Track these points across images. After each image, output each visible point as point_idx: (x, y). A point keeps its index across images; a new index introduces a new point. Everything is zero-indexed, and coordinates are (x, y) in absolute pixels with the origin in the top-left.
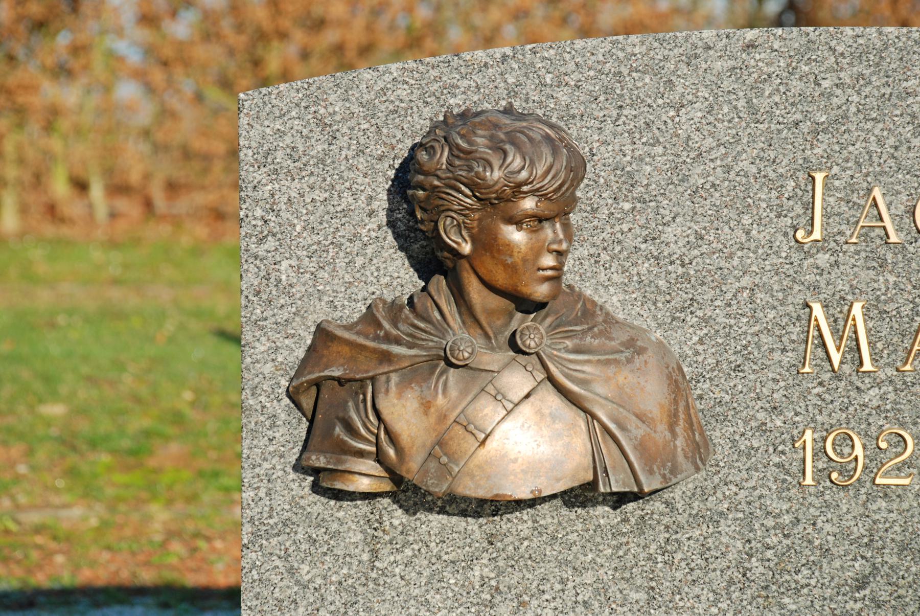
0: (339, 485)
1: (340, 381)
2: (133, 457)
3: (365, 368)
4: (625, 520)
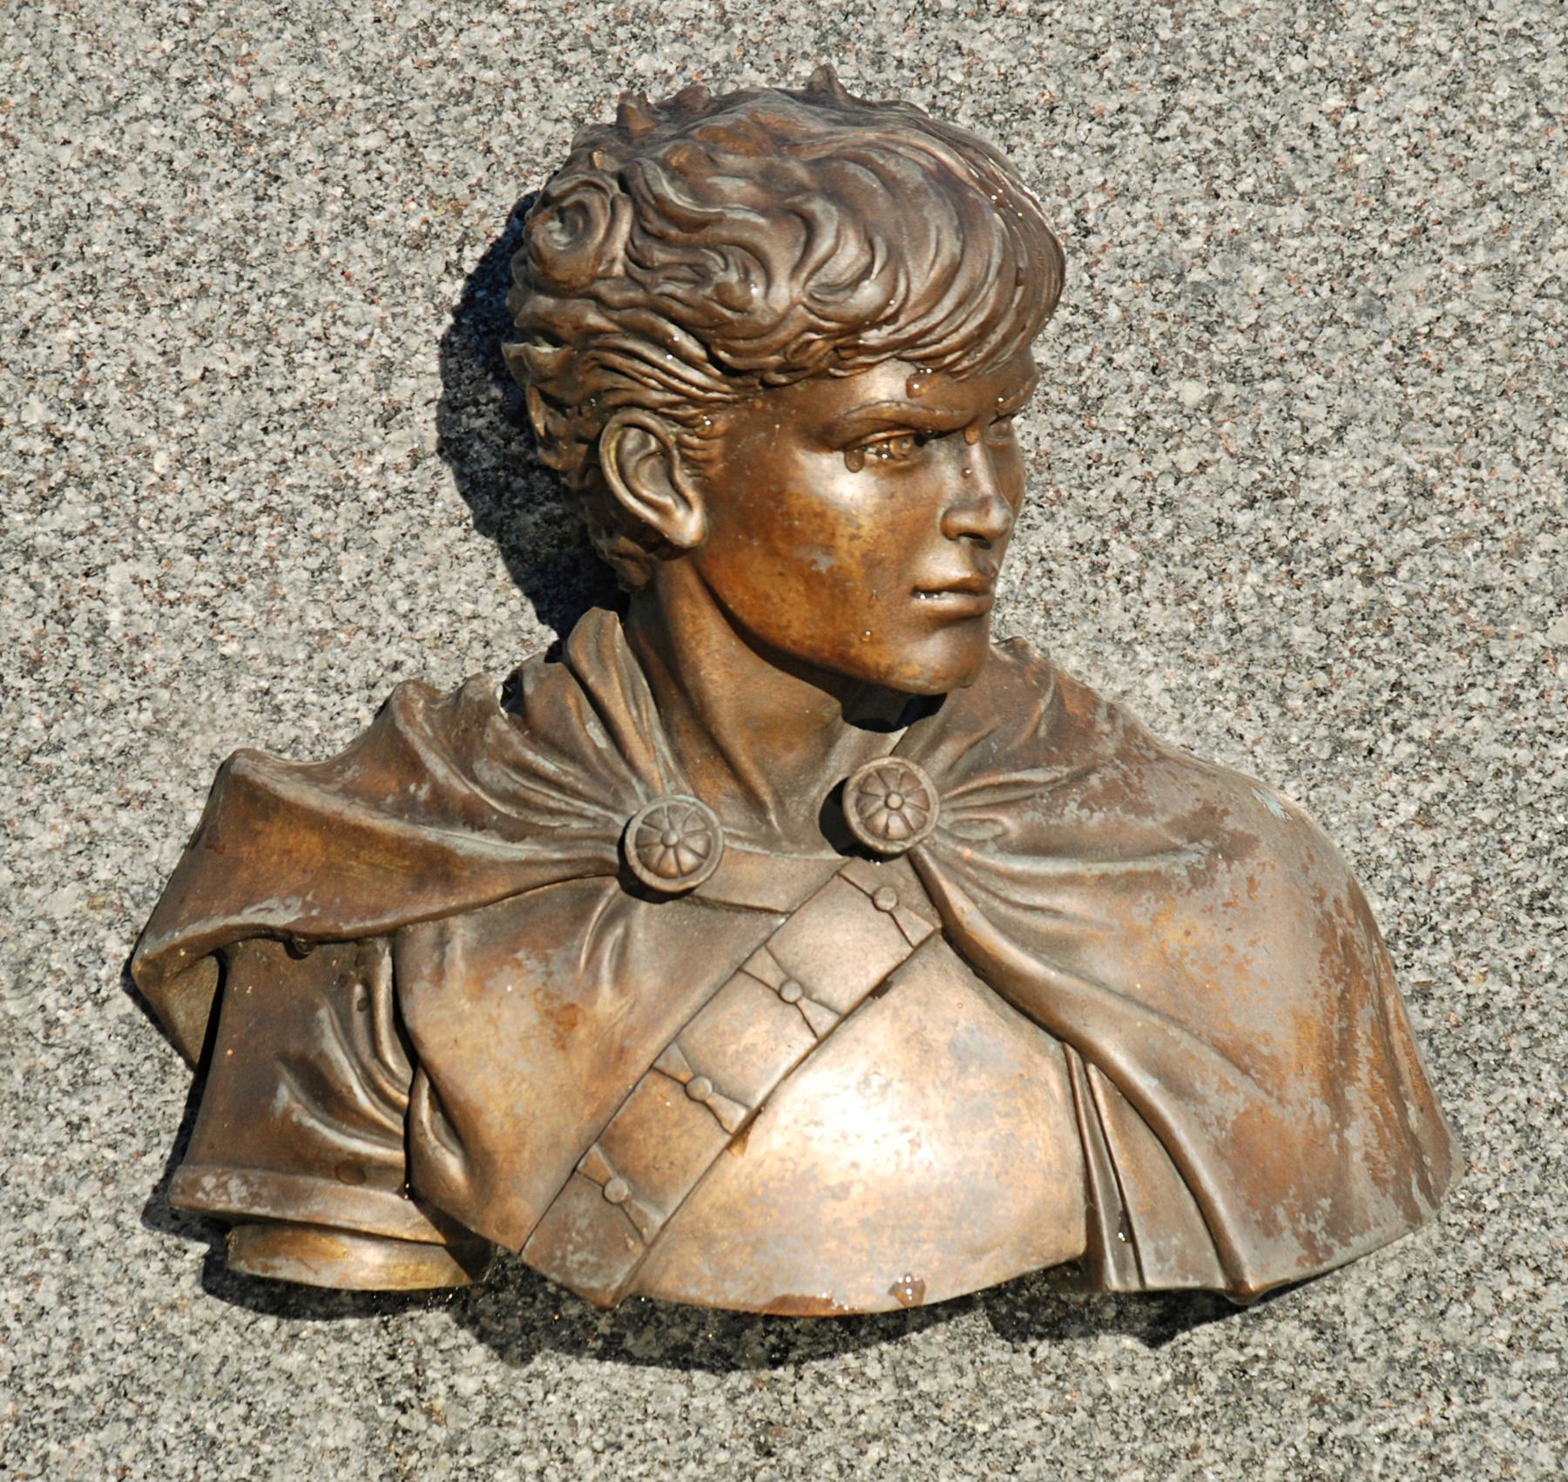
0: (287, 1270)
1: (292, 942)
4: (1187, 1380)
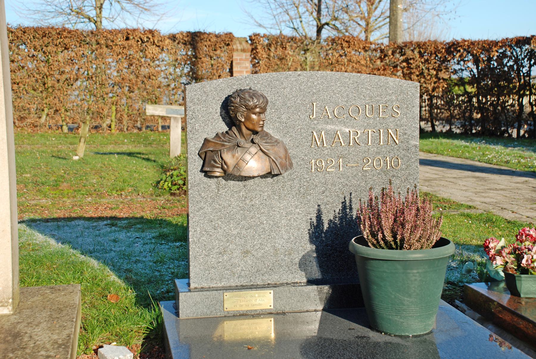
0: (212, 175)
1: (212, 151)
2: (56, 186)
3: (218, 148)
4: (274, 181)
